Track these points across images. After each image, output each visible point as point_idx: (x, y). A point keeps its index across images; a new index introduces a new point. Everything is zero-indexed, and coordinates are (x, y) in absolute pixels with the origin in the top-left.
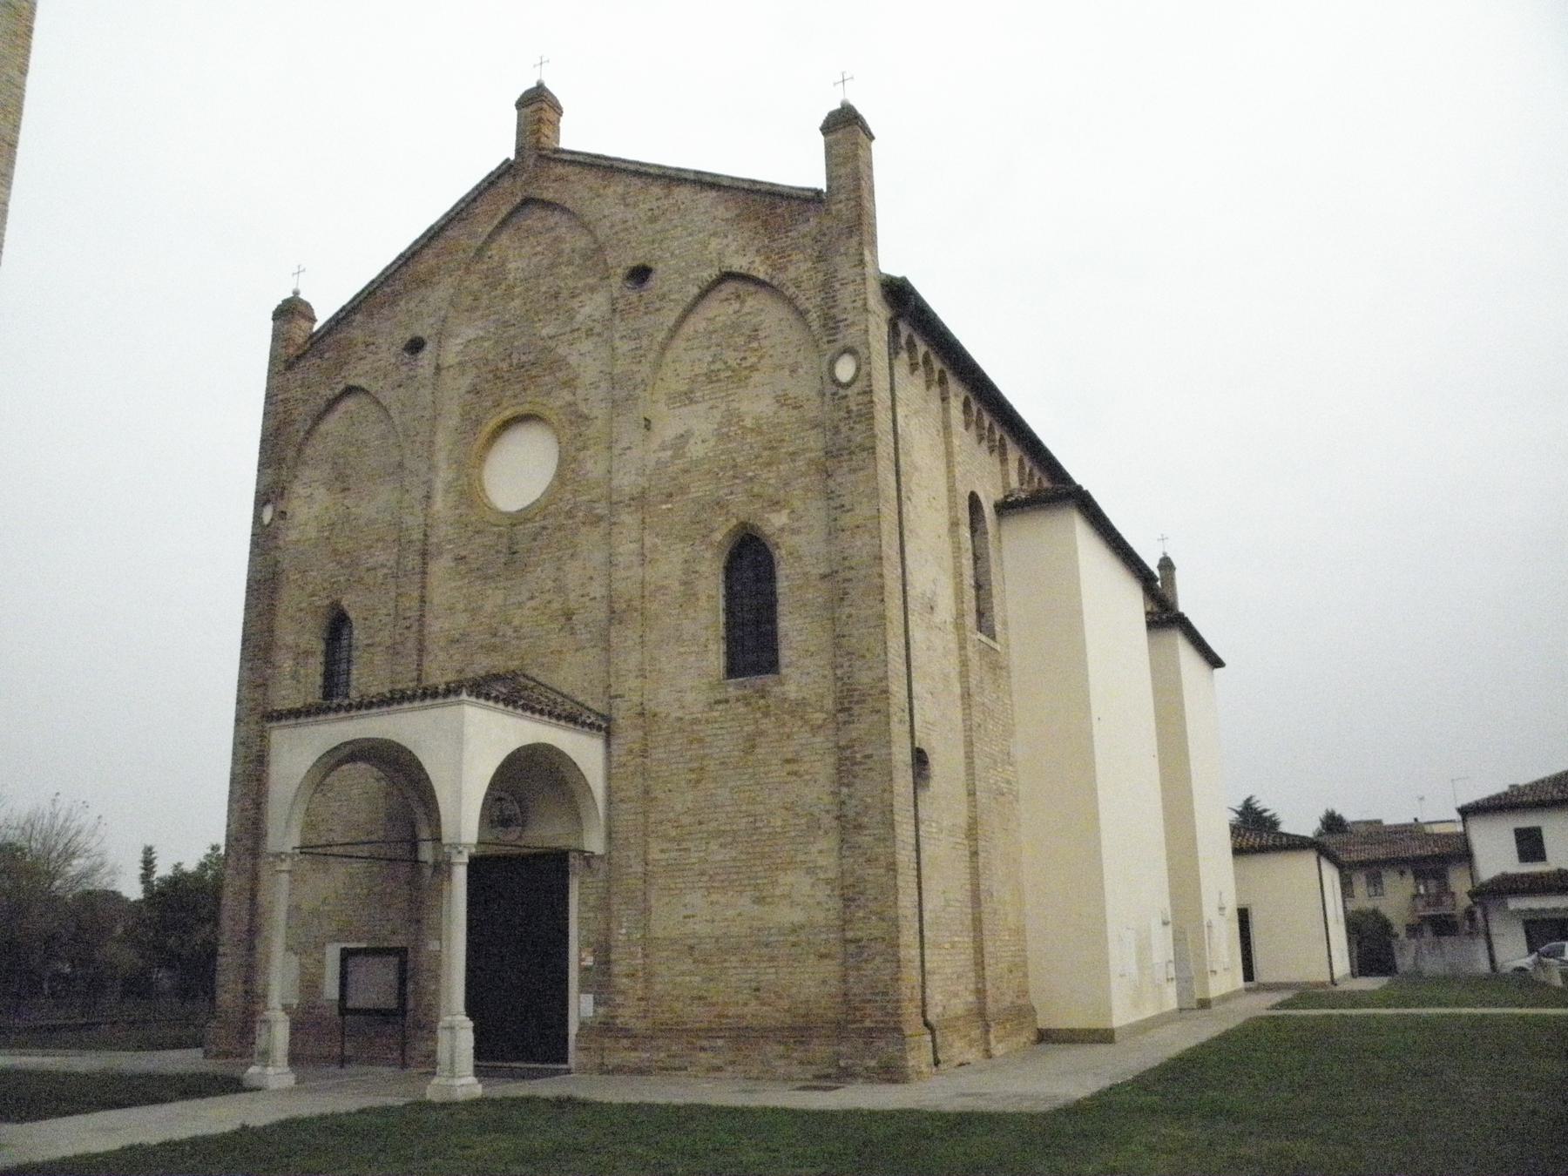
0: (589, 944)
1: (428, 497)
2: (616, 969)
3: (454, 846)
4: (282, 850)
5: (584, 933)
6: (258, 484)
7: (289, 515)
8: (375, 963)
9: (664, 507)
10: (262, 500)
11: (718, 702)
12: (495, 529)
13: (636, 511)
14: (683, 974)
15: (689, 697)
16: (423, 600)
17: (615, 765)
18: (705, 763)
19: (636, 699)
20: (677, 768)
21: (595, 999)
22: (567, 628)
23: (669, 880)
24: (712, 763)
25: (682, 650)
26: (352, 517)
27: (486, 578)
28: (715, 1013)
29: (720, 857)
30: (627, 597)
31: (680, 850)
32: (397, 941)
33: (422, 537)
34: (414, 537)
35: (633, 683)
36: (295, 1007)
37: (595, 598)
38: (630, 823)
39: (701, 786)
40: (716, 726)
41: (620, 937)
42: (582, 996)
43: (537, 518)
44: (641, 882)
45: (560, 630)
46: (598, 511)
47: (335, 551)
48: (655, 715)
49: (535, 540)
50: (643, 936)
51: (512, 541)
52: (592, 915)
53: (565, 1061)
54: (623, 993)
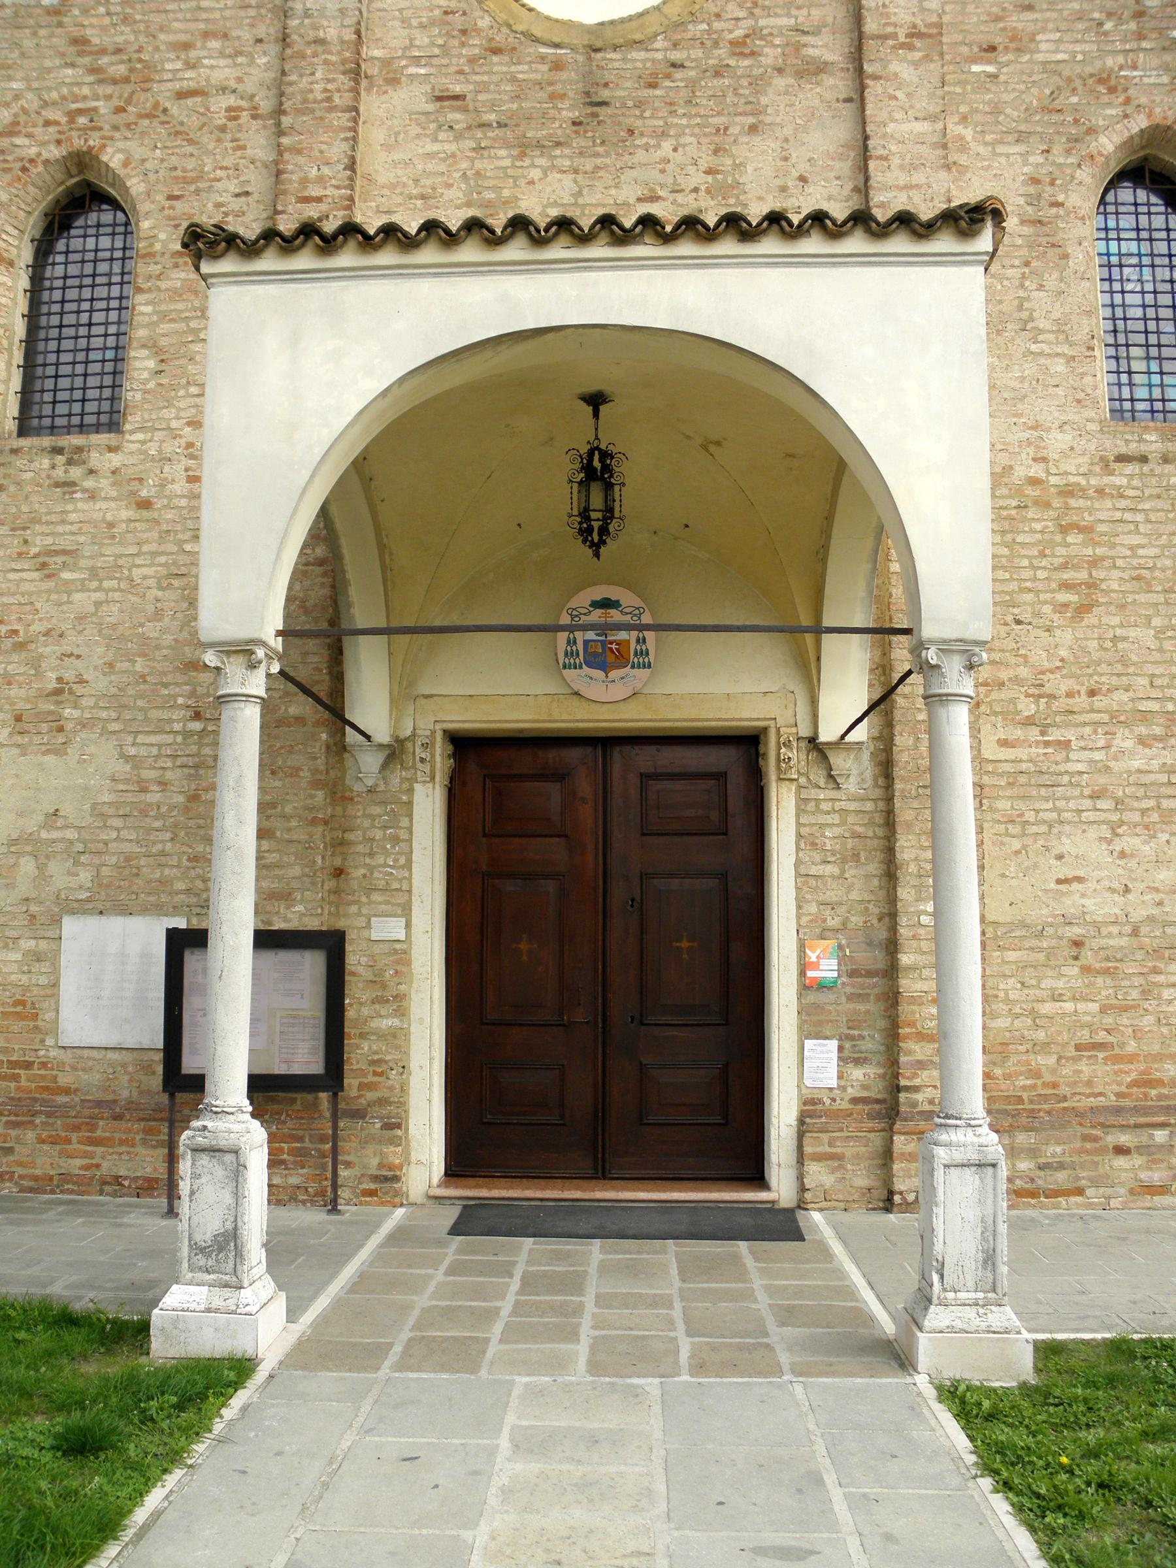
4: (255, 635)
5: (813, 908)
9: (975, 68)
11: (1121, 458)
13: (927, 58)
14: (1057, 998)
15: (1057, 441)
16: (352, 166)
18: (1098, 574)
20: (1035, 579)
21: (841, 1049)
23: (1021, 805)
24: (1116, 574)
27: (524, 148)
28: (1134, 1075)
29: (1136, 764)
31: (1047, 744)
33: (350, 36)
34: (331, 33)
39: (1091, 619)
40: (1122, 503)
42: (809, 1044)
43: (660, 43)
46: (811, 51)
47: (80, 42)
49: (653, 86)
53: (756, 1176)
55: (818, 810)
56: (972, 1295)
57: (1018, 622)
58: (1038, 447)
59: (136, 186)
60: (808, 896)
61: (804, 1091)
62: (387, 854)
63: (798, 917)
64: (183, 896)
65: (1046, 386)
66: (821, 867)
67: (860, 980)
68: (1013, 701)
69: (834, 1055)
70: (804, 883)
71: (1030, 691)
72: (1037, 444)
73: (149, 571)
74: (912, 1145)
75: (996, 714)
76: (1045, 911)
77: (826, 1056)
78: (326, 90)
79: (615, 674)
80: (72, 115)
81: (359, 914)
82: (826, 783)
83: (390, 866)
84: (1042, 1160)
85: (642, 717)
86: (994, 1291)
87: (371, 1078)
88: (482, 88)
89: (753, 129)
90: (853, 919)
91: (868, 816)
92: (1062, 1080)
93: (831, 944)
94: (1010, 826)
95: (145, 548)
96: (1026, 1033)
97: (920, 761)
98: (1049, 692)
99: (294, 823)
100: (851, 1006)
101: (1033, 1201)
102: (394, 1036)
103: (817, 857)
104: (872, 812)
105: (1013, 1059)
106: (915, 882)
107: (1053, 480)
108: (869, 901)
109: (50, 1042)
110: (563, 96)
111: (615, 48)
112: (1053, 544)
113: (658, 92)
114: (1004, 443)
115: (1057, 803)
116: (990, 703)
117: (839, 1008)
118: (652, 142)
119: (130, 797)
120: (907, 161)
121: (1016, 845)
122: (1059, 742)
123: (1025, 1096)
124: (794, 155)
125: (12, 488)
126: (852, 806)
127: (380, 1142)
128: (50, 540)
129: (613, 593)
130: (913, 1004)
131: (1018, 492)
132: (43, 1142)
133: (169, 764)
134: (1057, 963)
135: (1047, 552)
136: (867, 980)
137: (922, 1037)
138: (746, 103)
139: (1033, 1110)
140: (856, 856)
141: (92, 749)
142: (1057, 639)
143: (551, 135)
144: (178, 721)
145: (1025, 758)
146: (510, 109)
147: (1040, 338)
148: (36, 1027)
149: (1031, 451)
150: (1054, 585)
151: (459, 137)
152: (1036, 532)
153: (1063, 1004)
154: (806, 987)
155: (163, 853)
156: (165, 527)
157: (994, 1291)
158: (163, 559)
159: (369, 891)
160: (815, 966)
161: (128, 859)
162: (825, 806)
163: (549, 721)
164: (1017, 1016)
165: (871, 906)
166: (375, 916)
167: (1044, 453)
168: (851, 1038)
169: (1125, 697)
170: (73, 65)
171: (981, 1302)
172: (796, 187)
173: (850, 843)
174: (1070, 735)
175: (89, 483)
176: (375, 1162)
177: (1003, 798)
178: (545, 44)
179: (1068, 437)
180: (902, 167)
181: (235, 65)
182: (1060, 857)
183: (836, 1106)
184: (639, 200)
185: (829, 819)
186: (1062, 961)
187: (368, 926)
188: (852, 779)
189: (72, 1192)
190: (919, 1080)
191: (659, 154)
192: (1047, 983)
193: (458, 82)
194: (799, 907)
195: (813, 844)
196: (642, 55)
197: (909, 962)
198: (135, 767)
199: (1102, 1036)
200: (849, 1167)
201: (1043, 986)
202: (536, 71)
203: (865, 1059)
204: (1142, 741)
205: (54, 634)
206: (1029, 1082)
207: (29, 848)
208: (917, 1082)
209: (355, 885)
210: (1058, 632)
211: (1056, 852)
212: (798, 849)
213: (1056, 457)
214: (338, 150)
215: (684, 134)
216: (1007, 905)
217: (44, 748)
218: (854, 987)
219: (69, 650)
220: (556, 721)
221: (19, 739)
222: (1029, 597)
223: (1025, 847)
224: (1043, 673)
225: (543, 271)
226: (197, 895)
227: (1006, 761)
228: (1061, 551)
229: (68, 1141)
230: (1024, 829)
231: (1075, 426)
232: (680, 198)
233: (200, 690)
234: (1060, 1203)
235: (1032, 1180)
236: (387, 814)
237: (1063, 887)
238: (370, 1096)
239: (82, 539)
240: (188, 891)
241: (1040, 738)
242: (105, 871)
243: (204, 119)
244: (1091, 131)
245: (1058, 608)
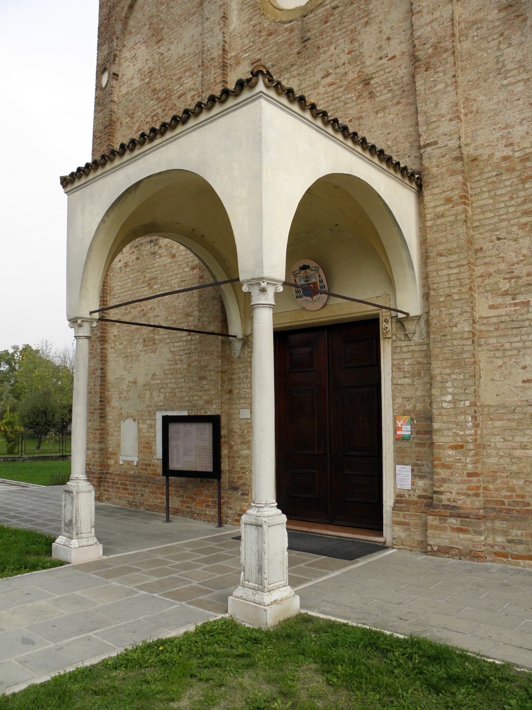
0: (405, 413)
1: (225, 17)
2: (438, 439)
3: (256, 281)
5: (400, 400)
6: (97, 60)
7: (120, 76)
8: (193, 428)
10: (101, 69)
12: (286, 26)
17: (428, 217)
19: (453, 143)
20: (507, 213)
21: (413, 470)
22: (366, 94)
23: (502, 340)
25: (505, 82)
26: (165, 60)
30: (433, 40)
31: (516, 304)
32: (212, 411)
33: (221, 52)
34: (215, 55)
35: (445, 127)
36: (135, 464)
37: (394, 57)
38: (452, 277)
41: (445, 405)
42: (398, 467)
44: (469, 342)
45: (358, 97)
48: (475, 159)
49: (326, 22)
50: (473, 404)
51: (304, 30)
52: (407, 381)
54: (449, 467)
55: (402, 352)
56: (254, 585)
57: (499, 239)
58: (508, 138)
60: (397, 395)
61: (397, 490)
62: (244, 383)
63: (393, 405)
64: (187, 403)
65: (512, 102)
66: (403, 380)
67: (422, 436)
68: (496, 283)
69: (410, 473)
70: (396, 388)
71: (506, 276)
73: (175, 281)
74: (436, 521)
75: (487, 291)
76: (516, 399)
77: (405, 473)
78: (215, 78)
79: (315, 297)
80: (152, 118)
81: (237, 408)
82: (405, 338)
83: (246, 388)
84: (510, 538)
85: (328, 316)
86: (261, 585)
87: (241, 475)
89: (367, 23)
90: (418, 405)
91: (424, 353)
92: (527, 494)
93: (408, 418)
94: (496, 353)
95: (174, 272)
96: (506, 466)
97: (442, 322)
98: (516, 275)
99: (212, 373)
100: (417, 449)
101: (504, 560)
102: (248, 458)
103: (401, 375)
104: (426, 350)
105: (499, 481)
106: (440, 385)
107: (517, 154)
108: (426, 396)
109: (154, 457)
110: (293, 43)
111: (312, 11)
112: (517, 191)
113: (328, 24)
114: (489, 142)
115: (523, 337)
116: (484, 286)
117: (412, 450)
118: (326, 49)
119: (173, 367)
120: (431, 8)
121: (500, 362)
122: (523, 303)
123: (506, 501)
124: (384, 28)
125: (141, 258)
126: (417, 348)
127: (240, 501)
128: (150, 275)
129: (307, 262)
130: (440, 449)
131: (498, 166)
132: (150, 493)
133: (182, 353)
134: (523, 427)
135: (514, 196)
136: (424, 436)
137: (445, 466)
138: (363, 12)
139: (510, 509)
140: (419, 374)
141: (162, 350)
142: (521, 244)
143: (290, 63)
144: (184, 337)
145: (504, 314)
146: (276, 58)
147: (509, 75)
148: (151, 452)
149: (504, 142)
150: (519, 214)
152: (508, 186)
153: (527, 451)
154: (398, 439)
155: (182, 387)
156: (179, 263)
157: (261, 585)
158: (179, 276)
159: (240, 398)
160: (400, 429)
161: (173, 390)
162: (405, 349)
163: (296, 322)
164: (502, 457)
165: (426, 399)
166: (241, 408)
167: (511, 141)
168: (417, 465)
170: (152, 100)
171: (256, 588)
172: (385, 44)
173: (416, 367)
175: (159, 252)
176: (239, 508)
177: (492, 337)
178: (287, 23)
179: (525, 127)
180: (428, 13)
181: (193, 79)
182: (524, 368)
183: (411, 499)
184: (322, 78)
185: (406, 356)
186: (526, 427)
187: (239, 413)
188: (417, 335)
189: (157, 511)
190: (443, 488)
191: (330, 53)
192: (517, 439)
193: (259, 54)
194: (394, 400)
195: (400, 369)
196: (322, 9)
197: (437, 427)
198: (174, 355)
200: (412, 529)
201: (515, 440)
202: (284, 36)
203: (424, 476)
205: (152, 309)
206: (508, 494)
207: (148, 387)
208: (442, 489)
209: (235, 396)
210: (521, 240)
211: (522, 365)
212: (393, 372)
213: (518, 141)
215: (339, 39)
216: (495, 396)
217: (151, 351)
218: (418, 439)
219: (156, 314)
220: (298, 321)
221: (145, 348)
222: (504, 224)
223: (505, 363)
224: (513, 265)
225: (136, 160)
226: (191, 402)
227: (494, 317)
228: (522, 194)
229: (156, 493)
230: (504, 353)
231: (529, 120)
232: (338, 71)
233: (190, 324)
234: (519, 563)
235: (504, 548)
236: (244, 367)
237: (526, 385)
238: (241, 482)
239: (158, 272)
240: (188, 401)
241: (512, 302)
242: (167, 394)
243: (185, 104)
245: (521, 226)
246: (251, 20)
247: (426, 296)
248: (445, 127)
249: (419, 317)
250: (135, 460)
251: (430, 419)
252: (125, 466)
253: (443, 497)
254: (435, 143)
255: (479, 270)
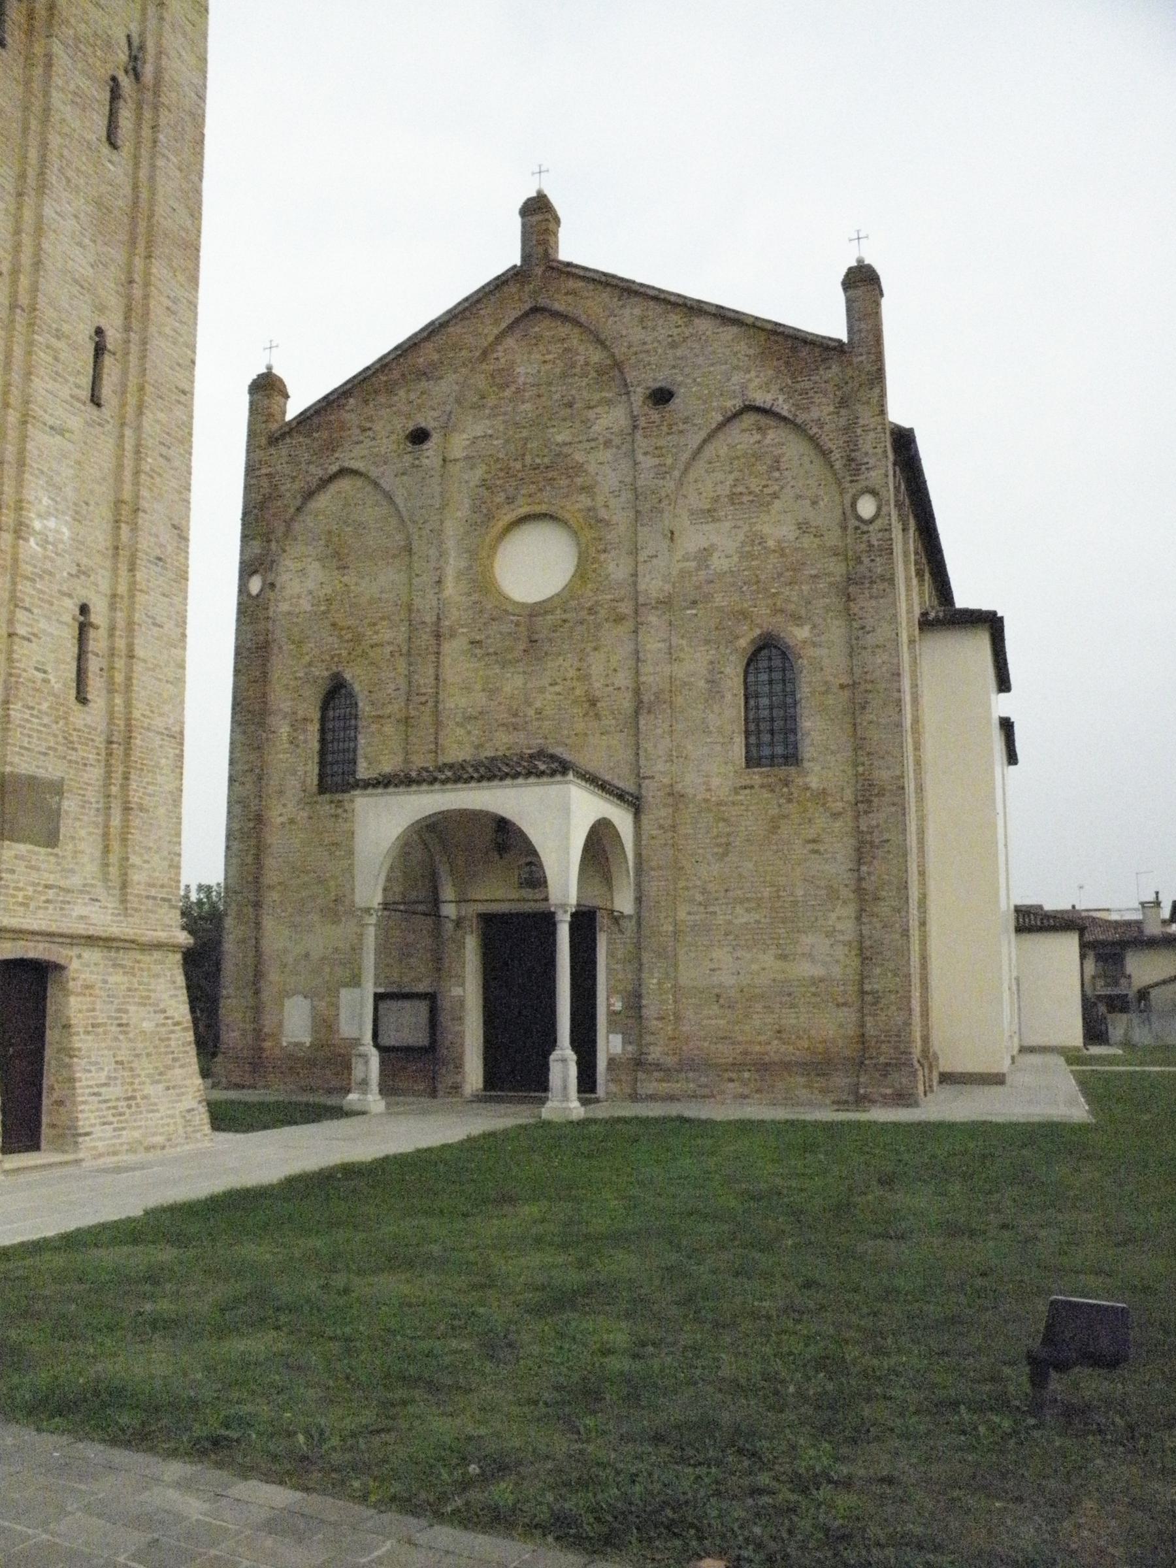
5: (613, 982)
9: (689, 612)
10: (247, 570)
15: (715, 782)
16: (437, 679)
17: (644, 837)
30: (655, 689)
34: (428, 619)
35: (660, 766)
39: (727, 859)
43: (558, 611)
47: (334, 625)
50: (674, 986)
59: (357, 688)
72: (706, 783)
88: (488, 637)
89: (595, 649)
151: (479, 660)
169: (739, 892)
174: (717, 909)
199: (728, 1034)
204: (748, 910)
214: (431, 671)
222: (700, 851)
244: (737, 637)
246: (469, 594)
247: (639, 900)
248: (660, 766)
249: (630, 917)
250: (307, 1040)
251: (640, 996)
252: (291, 1047)
253: (650, 1057)
254: (653, 777)
255: (681, 884)
